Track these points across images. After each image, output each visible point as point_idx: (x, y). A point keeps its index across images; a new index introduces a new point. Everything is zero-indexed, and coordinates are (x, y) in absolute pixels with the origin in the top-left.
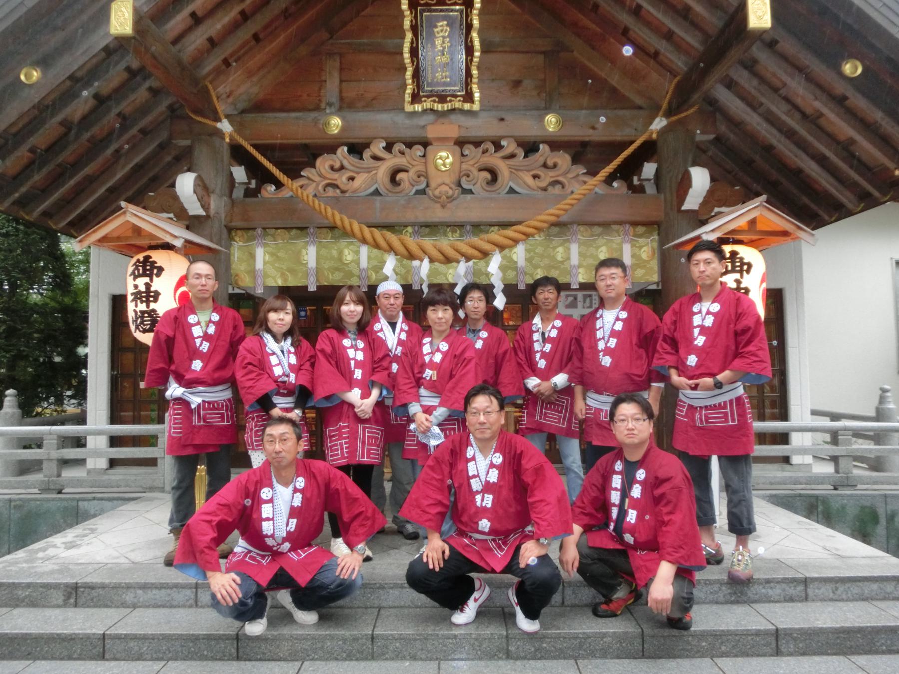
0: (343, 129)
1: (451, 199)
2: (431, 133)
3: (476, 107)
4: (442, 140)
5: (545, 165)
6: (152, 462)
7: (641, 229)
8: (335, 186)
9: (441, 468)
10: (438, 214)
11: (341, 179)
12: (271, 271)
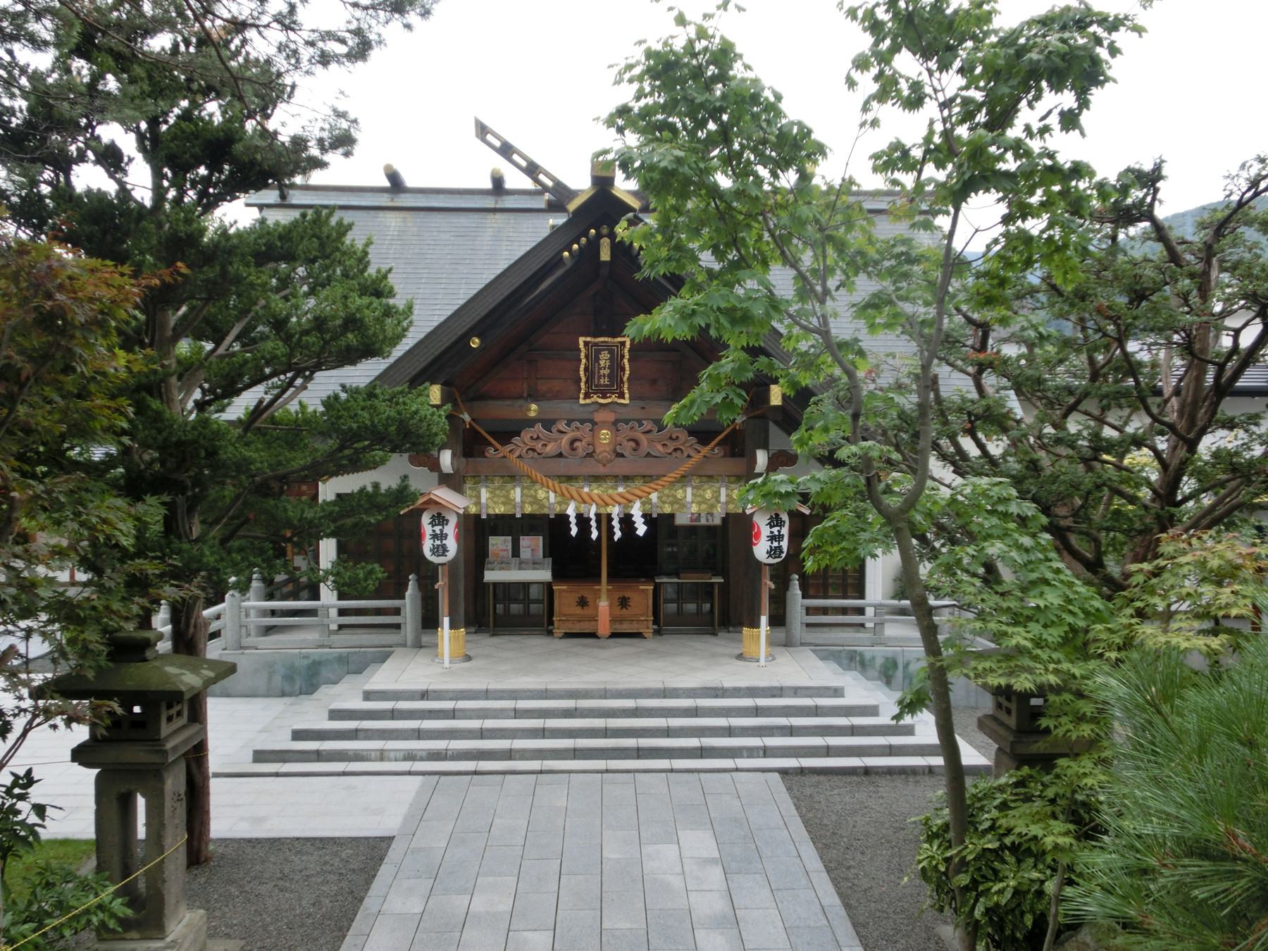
0: (539, 412)
1: (610, 461)
2: (600, 416)
3: (626, 401)
4: (604, 422)
5: (671, 438)
6: (397, 627)
7: (733, 479)
8: (534, 450)
9: (824, 252)
10: (601, 470)
11: (539, 446)
12: (491, 504)
